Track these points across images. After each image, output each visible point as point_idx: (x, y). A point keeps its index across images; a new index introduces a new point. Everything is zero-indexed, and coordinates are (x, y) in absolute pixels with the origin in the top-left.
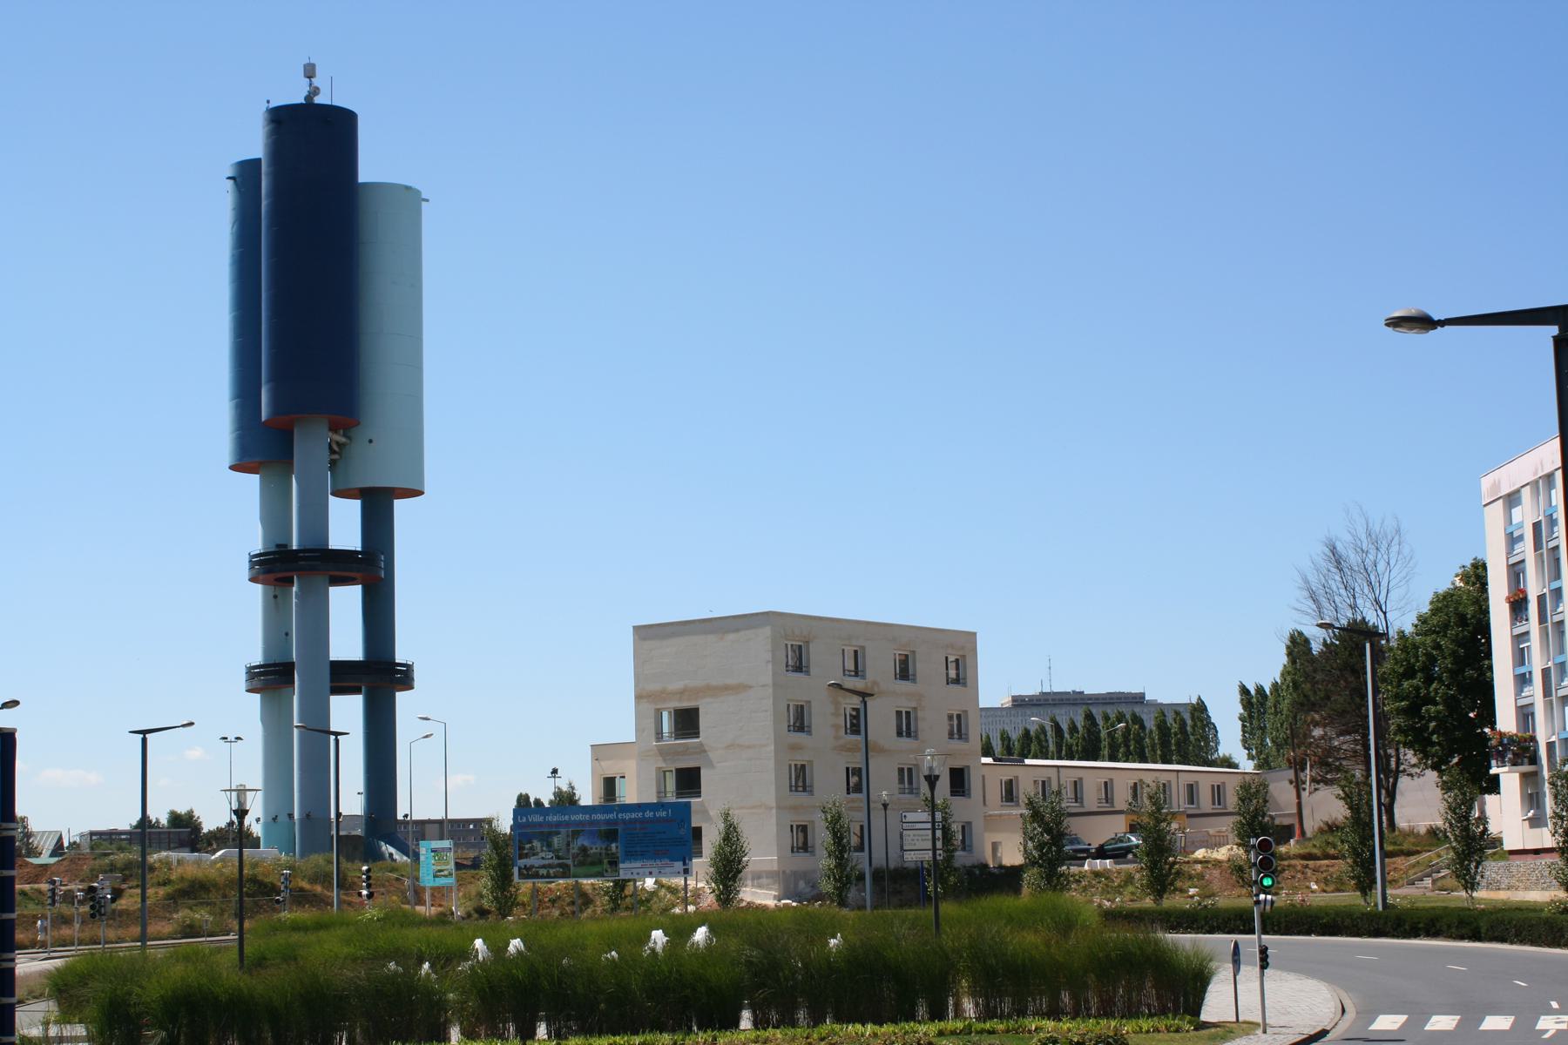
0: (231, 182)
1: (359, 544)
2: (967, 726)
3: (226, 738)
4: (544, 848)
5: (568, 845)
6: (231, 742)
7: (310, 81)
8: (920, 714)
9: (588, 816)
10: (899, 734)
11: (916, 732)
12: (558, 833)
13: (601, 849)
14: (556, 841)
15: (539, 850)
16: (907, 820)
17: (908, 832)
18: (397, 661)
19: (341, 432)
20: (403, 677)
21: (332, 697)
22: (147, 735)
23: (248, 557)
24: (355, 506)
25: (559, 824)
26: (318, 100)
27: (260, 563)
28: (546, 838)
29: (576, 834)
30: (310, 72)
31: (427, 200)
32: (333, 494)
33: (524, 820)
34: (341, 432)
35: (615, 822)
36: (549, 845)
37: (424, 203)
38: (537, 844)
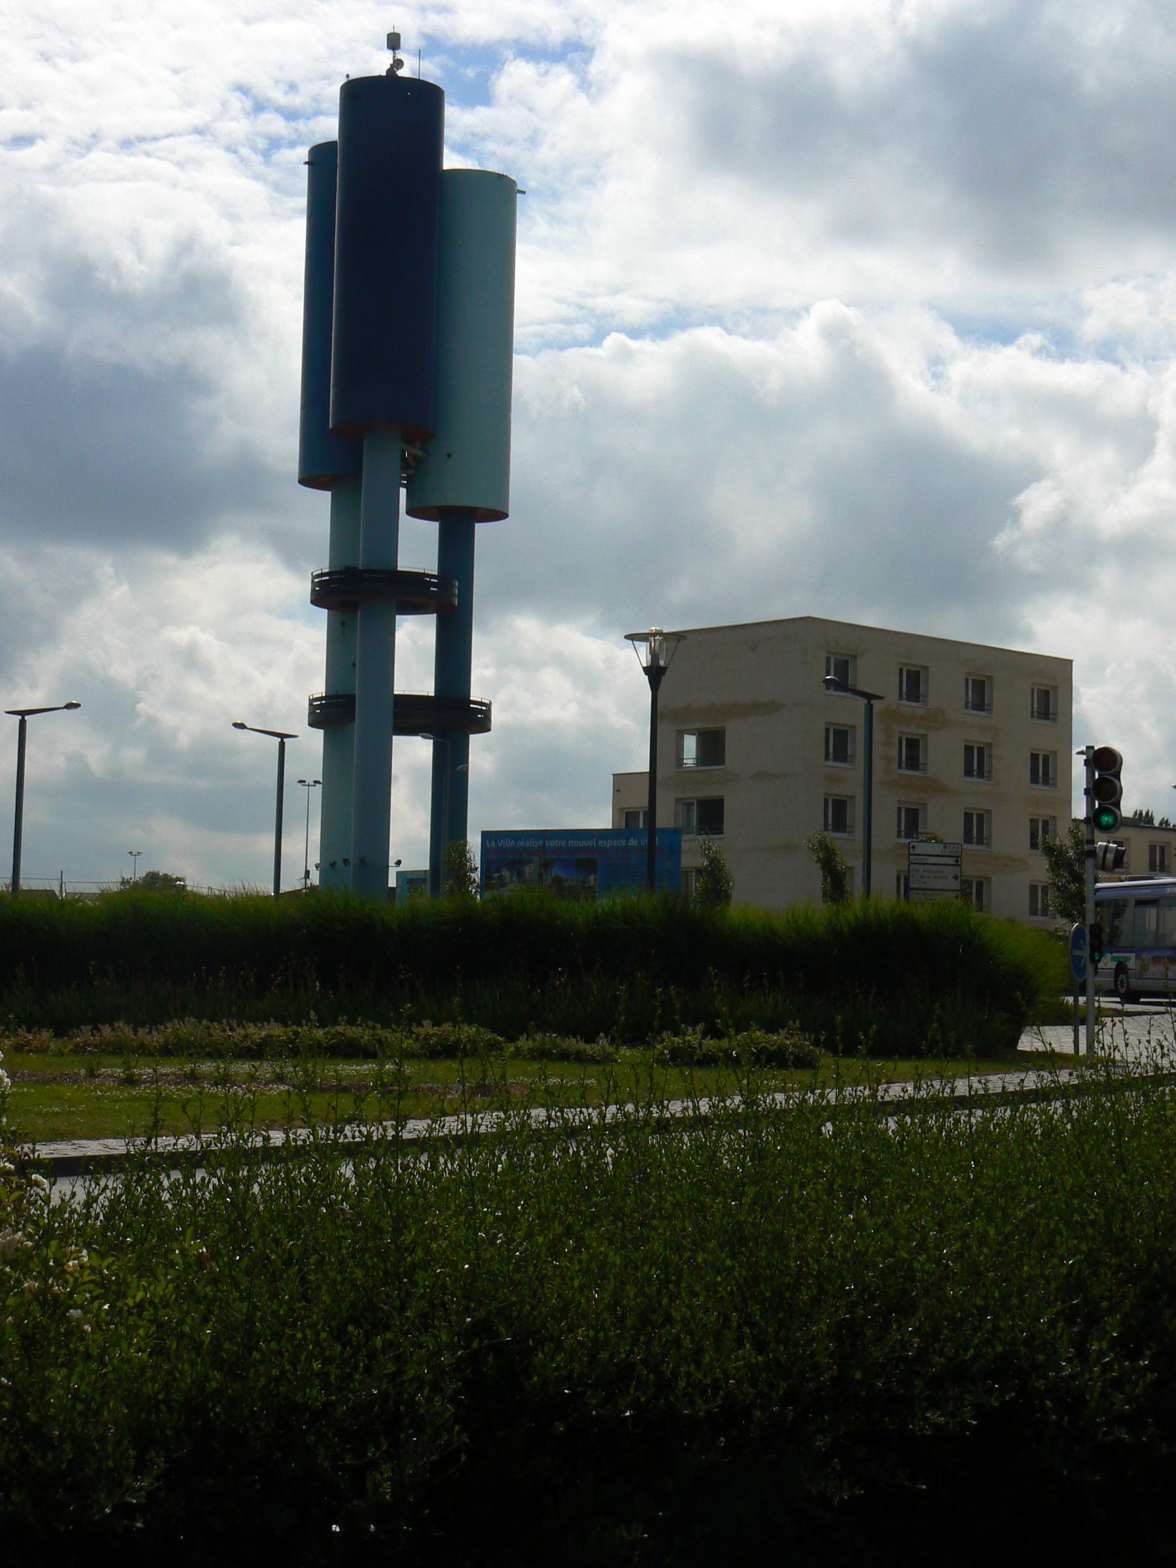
0: (307, 166)
1: (436, 568)
2: (1055, 769)
3: (304, 781)
4: (514, 879)
5: (541, 875)
6: (309, 785)
7: (394, 53)
8: (995, 751)
9: (565, 842)
10: (968, 772)
11: (990, 772)
12: (530, 861)
13: (578, 881)
15: (508, 880)
16: (915, 852)
17: (916, 867)
18: (472, 698)
19: (418, 444)
20: (479, 719)
21: (394, 737)
22: (26, 718)
23: (310, 577)
24: (431, 529)
26: (402, 73)
27: (320, 584)
29: (546, 865)
30: (394, 41)
31: (523, 193)
32: (411, 512)
33: (493, 844)
34: (418, 444)
36: (520, 875)
37: (518, 195)
38: (505, 873)
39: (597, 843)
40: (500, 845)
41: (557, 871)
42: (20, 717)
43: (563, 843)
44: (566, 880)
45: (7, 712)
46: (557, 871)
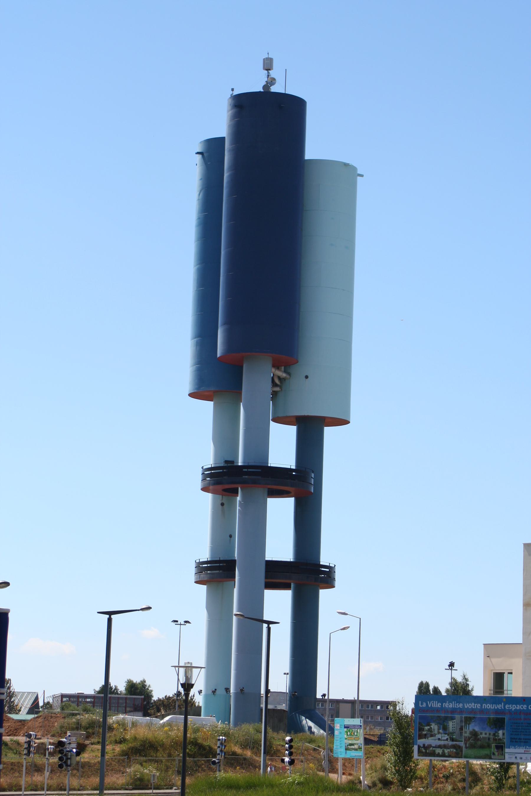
3: (177, 621)
4: (441, 731)
5: (461, 729)
6: (181, 624)
12: (453, 718)
13: (490, 734)
14: (451, 724)
18: (321, 563)
19: (283, 368)
22: (112, 616)
25: (453, 711)
26: (274, 89)
28: (443, 723)
29: (468, 720)
31: (362, 176)
34: (283, 368)
35: (503, 712)
36: (445, 728)
38: (434, 727)
39: (504, 707)
40: (430, 706)
41: (473, 727)
42: (108, 616)
43: (479, 706)
44: (481, 734)
45: (98, 613)
46: (473, 727)
